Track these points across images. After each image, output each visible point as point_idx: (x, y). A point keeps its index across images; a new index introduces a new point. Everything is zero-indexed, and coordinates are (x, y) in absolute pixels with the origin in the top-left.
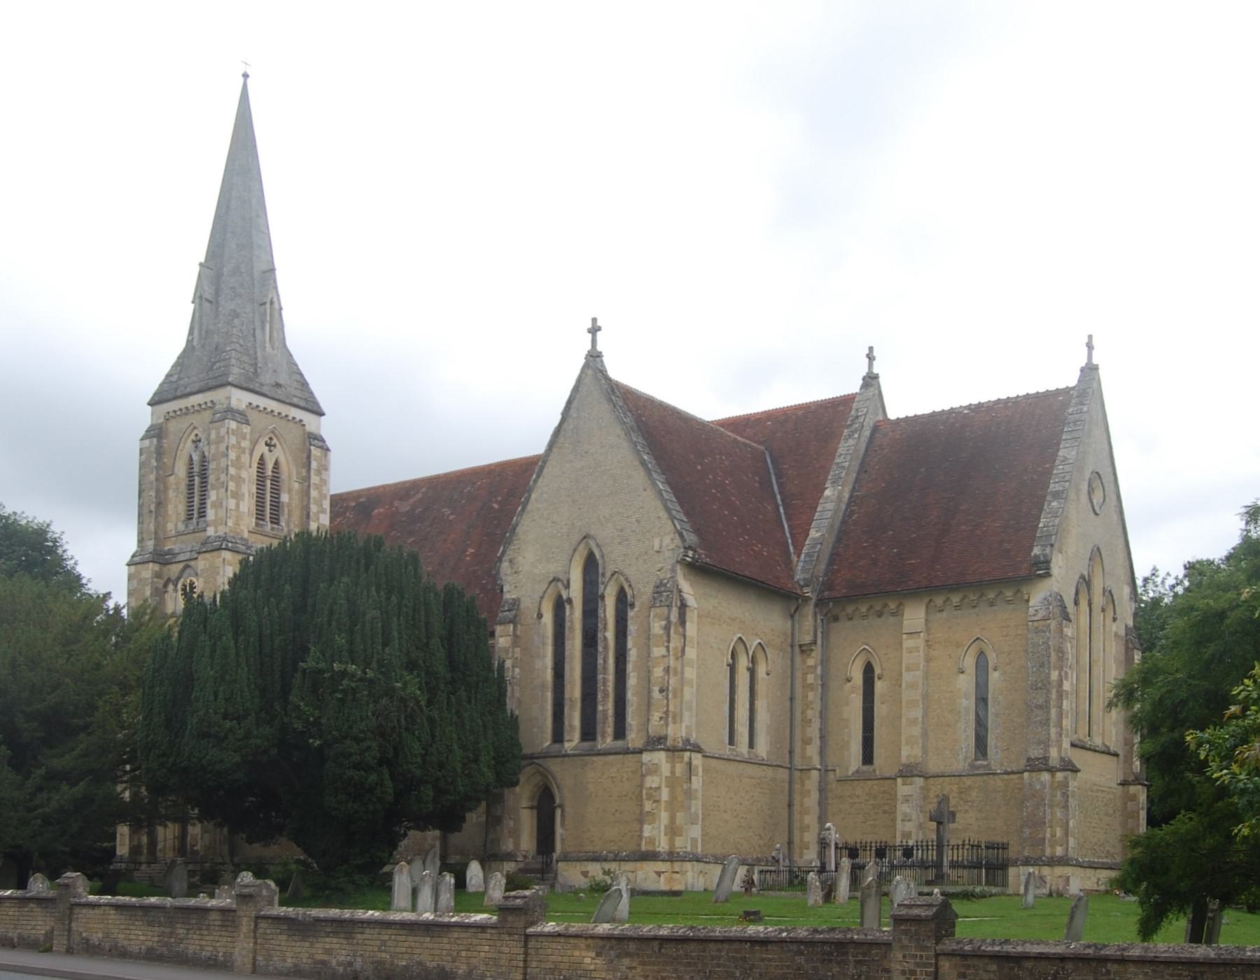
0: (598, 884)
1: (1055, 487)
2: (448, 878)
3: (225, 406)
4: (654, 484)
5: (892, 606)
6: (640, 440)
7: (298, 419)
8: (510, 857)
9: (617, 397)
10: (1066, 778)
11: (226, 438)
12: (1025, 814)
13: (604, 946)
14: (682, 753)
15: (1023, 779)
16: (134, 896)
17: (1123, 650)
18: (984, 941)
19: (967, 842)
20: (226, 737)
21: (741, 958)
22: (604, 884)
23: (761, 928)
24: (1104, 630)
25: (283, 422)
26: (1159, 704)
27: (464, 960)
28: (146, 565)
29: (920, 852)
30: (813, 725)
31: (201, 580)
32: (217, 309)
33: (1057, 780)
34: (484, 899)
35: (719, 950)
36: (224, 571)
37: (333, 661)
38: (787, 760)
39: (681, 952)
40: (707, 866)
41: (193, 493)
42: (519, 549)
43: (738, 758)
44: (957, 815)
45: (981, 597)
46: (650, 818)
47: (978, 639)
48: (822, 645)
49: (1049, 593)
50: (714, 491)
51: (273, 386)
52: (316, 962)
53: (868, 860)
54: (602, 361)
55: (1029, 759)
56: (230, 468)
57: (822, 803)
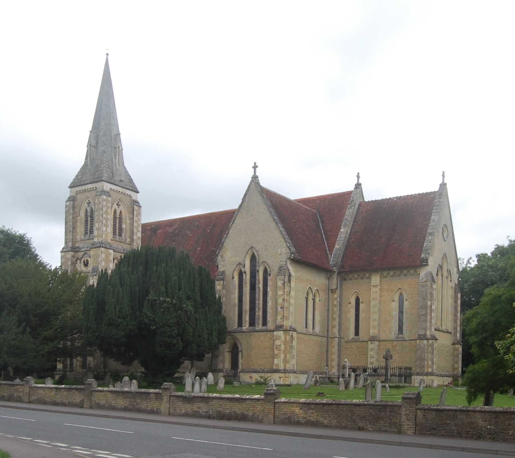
0: (258, 382)
1: (430, 231)
3: (101, 189)
4: (279, 228)
5: (367, 275)
6: (273, 211)
7: (129, 194)
8: (221, 371)
9: (264, 193)
12: (417, 356)
13: (303, 406)
14: (289, 332)
15: (417, 342)
16: (218, 394)
17: (454, 293)
19: (397, 367)
20: (119, 325)
21: (351, 410)
23: (358, 401)
25: (123, 196)
28: (69, 253)
31: (92, 259)
32: (97, 150)
33: (429, 343)
35: (343, 408)
37: (160, 297)
38: (326, 334)
39: (330, 408)
42: (225, 251)
45: (401, 272)
46: (277, 356)
47: (400, 288)
48: (340, 290)
49: (427, 272)
50: (299, 230)
51: (120, 181)
52: (194, 411)
54: (258, 180)
55: (419, 335)
56: (104, 215)
57: (339, 350)
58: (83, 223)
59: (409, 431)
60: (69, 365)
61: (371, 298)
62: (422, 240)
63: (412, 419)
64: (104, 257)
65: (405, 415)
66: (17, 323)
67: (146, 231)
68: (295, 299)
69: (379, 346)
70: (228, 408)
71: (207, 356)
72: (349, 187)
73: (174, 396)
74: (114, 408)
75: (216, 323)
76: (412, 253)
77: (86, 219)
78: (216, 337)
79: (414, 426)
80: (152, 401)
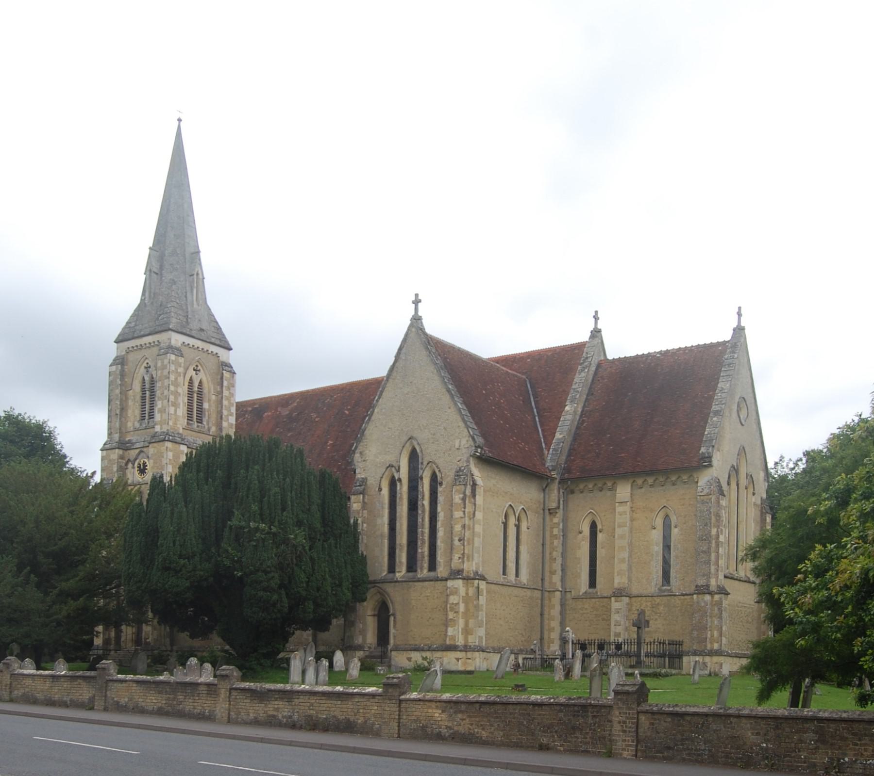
0: (419, 666)
2: (324, 662)
3: (167, 344)
4: (456, 404)
5: (609, 484)
6: (447, 375)
8: (360, 648)
10: (721, 599)
11: (168, 366)
12: (694, 622)
13: (447, 706)
18: (664, 705)
19: (656, 640)
20: (181, 570)
22: (422, 666)
23: (539, 697)
24: (747, 501)
25: (205, 355)
26: (770, 561)
27: (361, 715)
28: (114, 451)
29: (626, 646)
30: (557, 562)
31: (151, 461)
32: (161, 278)
34: (346, 676)
35: (515, 709)
36: (167, 455)
37: (250, 521)
38: (540, 585)
39: (492, 710)
40: (489, 655)
41: (145, 402)
42: (366, 445)
43: (508, 584)
44: (650, 622)
45: (667, 479)
46: (452, 623)
47: (664, 506)
52: (269, 716)
53: (593, 651)
54: (422, 323)
55: (697, 586)
56: (171, 386)
57: (563, 613)
58: (137, 402)
59: (626, 753)
60: (113, 639)
61: (616, 524)
62: (702, 424)
63: (630, 729)
64: (171, 458)
65: (619, 722)
66: (15, 569)
67: (244, 415)
68: (484, 525)
69: (630, 605)
70: (325, 710)
71: (334, 621)
72: (582, 336)
73: (236, 689)
74: (141, 711)
75: (349, 566)
76: (684, 446)
77: (143, 394)
78: (348, 590)
79: (633, 742)
80: (202, 698)
